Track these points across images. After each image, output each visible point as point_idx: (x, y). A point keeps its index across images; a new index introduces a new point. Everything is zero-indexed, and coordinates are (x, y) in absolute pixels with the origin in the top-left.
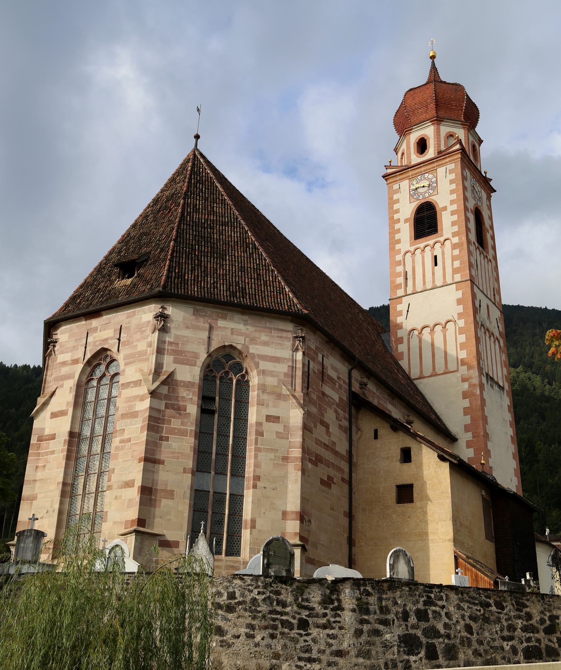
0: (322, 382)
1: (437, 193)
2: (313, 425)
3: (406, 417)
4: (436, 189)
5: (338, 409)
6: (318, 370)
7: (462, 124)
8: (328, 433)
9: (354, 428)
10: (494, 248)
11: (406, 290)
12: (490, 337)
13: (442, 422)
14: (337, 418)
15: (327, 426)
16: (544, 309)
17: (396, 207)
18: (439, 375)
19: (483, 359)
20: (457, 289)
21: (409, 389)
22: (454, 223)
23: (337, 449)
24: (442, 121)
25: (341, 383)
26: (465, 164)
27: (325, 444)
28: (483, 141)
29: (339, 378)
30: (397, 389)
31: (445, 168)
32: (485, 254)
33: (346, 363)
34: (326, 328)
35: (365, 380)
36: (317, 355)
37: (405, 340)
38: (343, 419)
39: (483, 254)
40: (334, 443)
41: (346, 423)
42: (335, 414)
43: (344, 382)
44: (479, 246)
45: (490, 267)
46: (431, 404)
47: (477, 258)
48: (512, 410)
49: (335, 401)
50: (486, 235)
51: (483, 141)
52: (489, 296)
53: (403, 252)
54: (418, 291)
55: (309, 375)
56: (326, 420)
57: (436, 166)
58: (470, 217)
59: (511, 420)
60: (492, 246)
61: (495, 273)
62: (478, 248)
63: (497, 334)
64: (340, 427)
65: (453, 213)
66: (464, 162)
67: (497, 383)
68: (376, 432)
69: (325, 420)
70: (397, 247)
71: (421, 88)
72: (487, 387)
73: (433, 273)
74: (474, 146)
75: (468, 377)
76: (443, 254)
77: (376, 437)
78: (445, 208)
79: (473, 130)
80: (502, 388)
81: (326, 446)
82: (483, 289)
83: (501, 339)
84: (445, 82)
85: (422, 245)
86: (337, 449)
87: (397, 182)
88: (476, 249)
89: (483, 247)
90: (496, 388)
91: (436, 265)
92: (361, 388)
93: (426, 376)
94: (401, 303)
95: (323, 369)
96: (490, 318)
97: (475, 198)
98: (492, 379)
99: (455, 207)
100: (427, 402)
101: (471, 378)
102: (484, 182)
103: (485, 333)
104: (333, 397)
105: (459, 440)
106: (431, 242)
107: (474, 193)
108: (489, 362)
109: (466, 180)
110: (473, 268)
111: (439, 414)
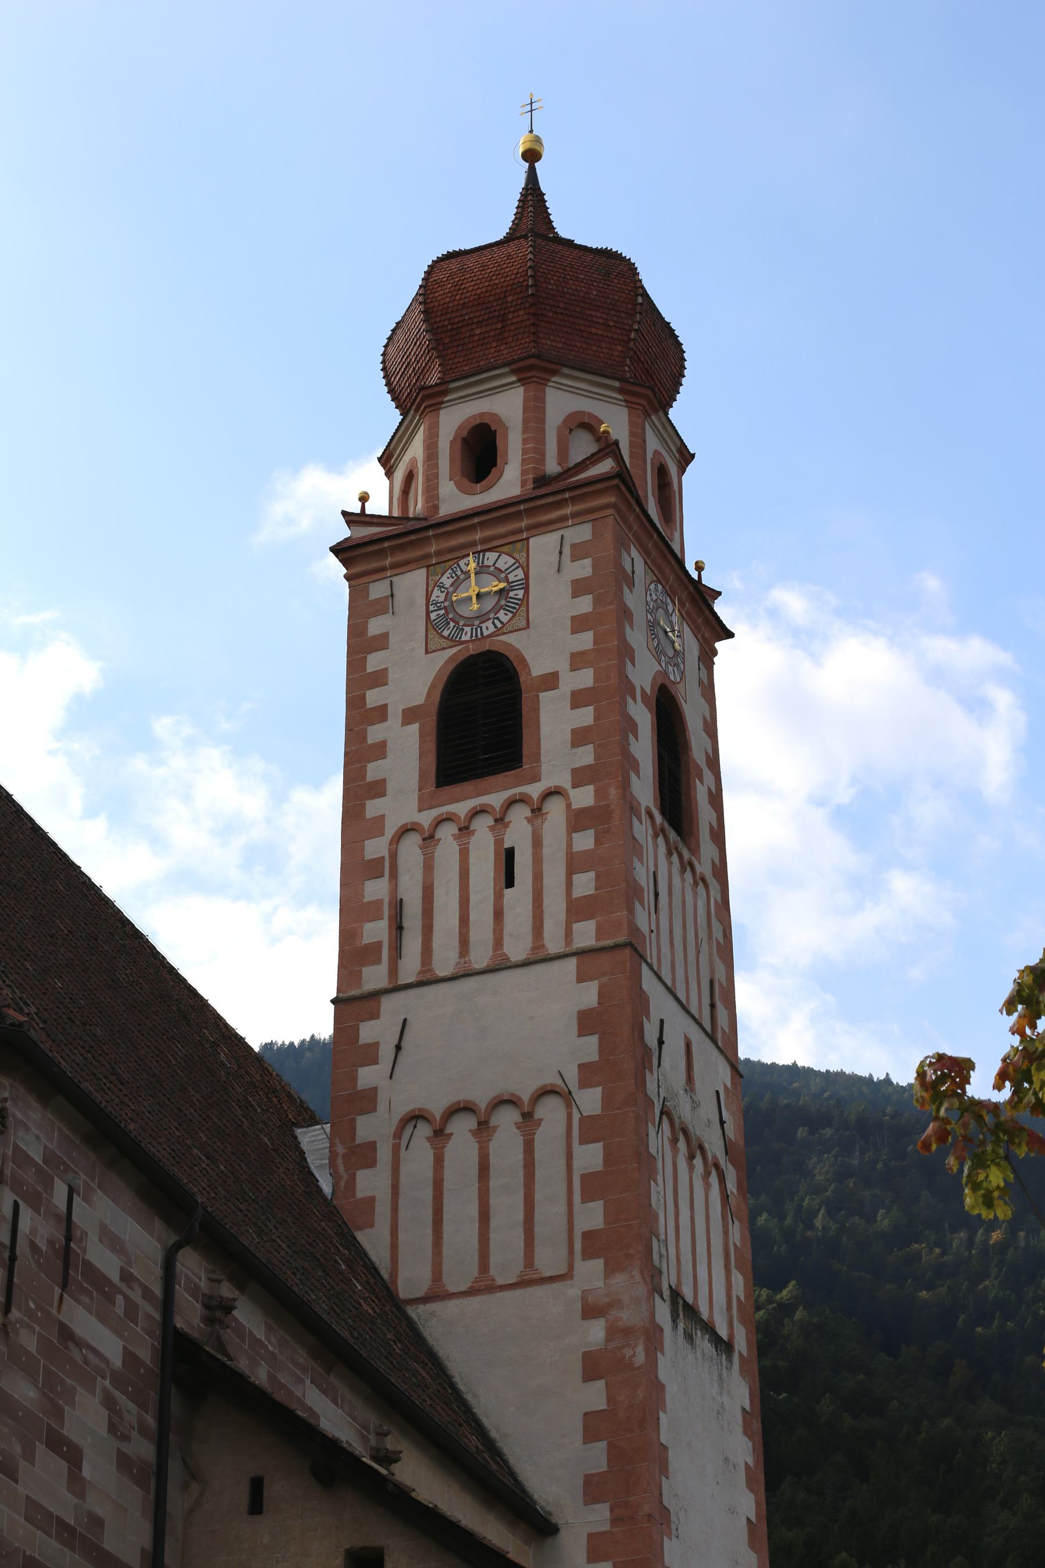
0: (64, 1286)
1: (523, 624)
2: (18, 1449)
3: (372, 1437)
4: (523, 608)
5: (117, 1393)
6: (51, 1242)
7: (621, 391)
8: (76, 1482)
9: (175, 1469)
10: (718, 836)
11: (393, 971)
12: (691, 1157)
13: (506, 1462)
14: (112, 1428)
15: (73, 1456)
16: (880, 1082)
17: (374, 662)
18: (502, 1288)
19: (662, 1237)
20: (582, 978)
21: (390, 1336)
22: (579, 738)
23: (109, 1543)
24: (555, 373)
25: (136, 1296)
26: (630, 528)
27: (60, 1522)
28: (693, 456)
29: (126, 1277)
30: (345, 1334)
31: (555, 536)
32: (686, 854)
33: (158, 1225)
34: (87, 1086)
35: (227, 1291)
36: (49, 1185)
37: (384, 1154)
38: (135, 1434)
39: (680, 856)
40: (97, 1523)
41: (144, 1450)
42: (106, 1413)
43: (147, 1294)
44: (666, 825)
45: (701, 904)
46: (468, 1397)
47: (656, 866)
48: (757, 1426)
49: (107, 1362)
50: (690, 789)
51: (693, 456)
52: (694, 1010)
53: (390, 831)
54: (441, 973)
55: (13, 1258)
56: (70, 1431)
57: (529, 528)
58: (637, 719)
59: (750, 1461)
60: (711, 828)
61: (716, 926)
62: (663, 830)
63: (715, 1148)
64: (124, 1462)
65: (578, 699)
66: (625, 521)
67: (709, 1329)
68: (257, 1487)
69: (65, 1432)
70: (373, 808)
71: (485, 252)
72: (672, 1339)
73: (498, 914)
74: (662, 472)
75: (606, 1300)
76: (537, 843)
77: (256, 1506)
78: (551, 681)
79: (661, 413)
80: (724, 1346)
81: (65, 1532)
82: (674, 980)
83: (730, 1166)
84: (570, 243)
85: (462, 808)
86: (106, 1546)
87: (383, 575)
88: (656, 836)
89: (679, 833)
90: (704, 1344)
91: (510, 883)
92: (210, 1321)
93: (452, 1289)
94: (375, 1015)
95: (69, 1238)
96: (692, 1090)
97: (658, 653)
98: (691, 1311)
99: (586, 678)
100: (452, 1385)
101: (615, 1303)
102: (693, 600)
103: (674, 1141)
104: (101, 1349)
105: (563, 1533)
106: (496, 800)
107: (657, 636)
108: (682, 1249)
109: (631, 585)
110: (642, 903)
111: (494, 1434)
